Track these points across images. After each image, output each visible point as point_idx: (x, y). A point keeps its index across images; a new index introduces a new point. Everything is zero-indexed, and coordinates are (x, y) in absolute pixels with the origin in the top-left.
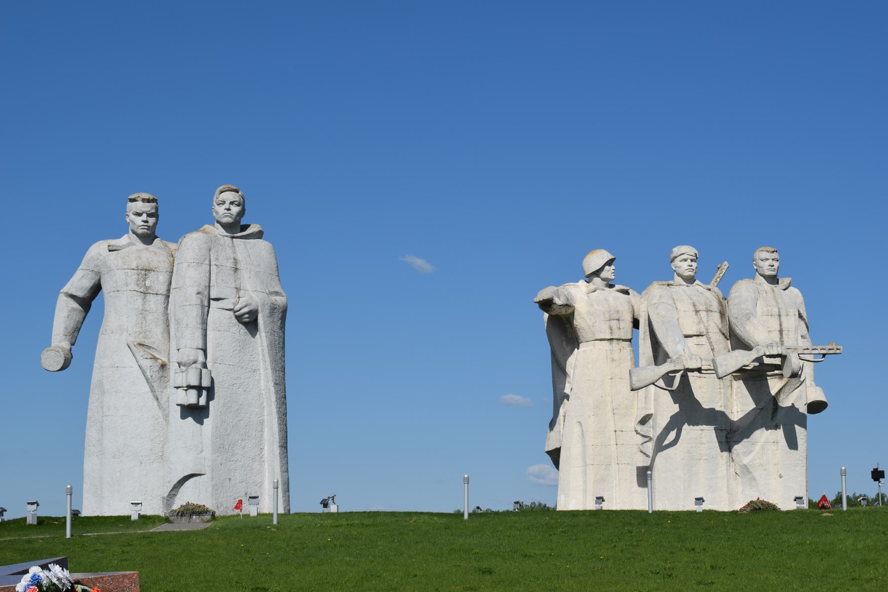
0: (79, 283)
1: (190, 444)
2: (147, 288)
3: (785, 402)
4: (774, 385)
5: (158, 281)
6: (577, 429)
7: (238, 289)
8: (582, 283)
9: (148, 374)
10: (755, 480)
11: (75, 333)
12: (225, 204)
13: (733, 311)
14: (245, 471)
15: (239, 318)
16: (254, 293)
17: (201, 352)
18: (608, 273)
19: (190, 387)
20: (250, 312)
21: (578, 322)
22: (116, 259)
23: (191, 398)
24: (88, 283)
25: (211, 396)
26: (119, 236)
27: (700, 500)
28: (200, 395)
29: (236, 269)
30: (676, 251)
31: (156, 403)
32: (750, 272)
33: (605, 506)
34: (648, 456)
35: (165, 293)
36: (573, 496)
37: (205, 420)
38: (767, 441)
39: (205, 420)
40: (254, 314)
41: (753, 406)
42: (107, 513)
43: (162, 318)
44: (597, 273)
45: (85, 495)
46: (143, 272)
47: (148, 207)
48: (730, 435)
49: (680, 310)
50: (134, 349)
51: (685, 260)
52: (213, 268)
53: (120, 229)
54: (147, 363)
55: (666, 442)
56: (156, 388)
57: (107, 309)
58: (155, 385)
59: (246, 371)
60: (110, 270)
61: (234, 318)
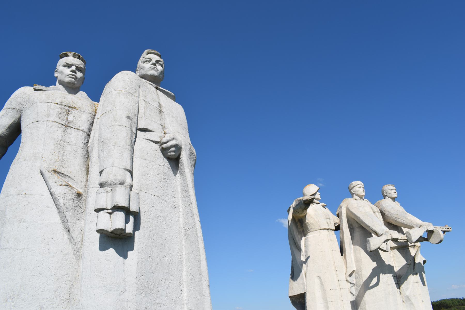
2: (69, 122)
6: (317, 281)
7: (163, 127)
9: (61, 202)
10: (412, 304)
15: (164, 151)
17: (129, 174)
19: (117, 208)
20: (176, 146)
23: (118, 221)
25: (137, 227)
28: (127, 221)
29: (161, 111)
30: (354, 183)
31: (66, 236)
34: (353, 295)
35: (86, 130)
37: (129, 253)
39: (129, 253)
41: (406, 263)
43: (81, 153)
46: (67, 108)
48: (399, 280)
50: (47, 175)
51: (360, 187)
52: (142, 103)
53: (49, 80)
54: (59, 191)
55: (371, 285)
56: (69, 218)
58: (68, 214)
61: (159, 151)
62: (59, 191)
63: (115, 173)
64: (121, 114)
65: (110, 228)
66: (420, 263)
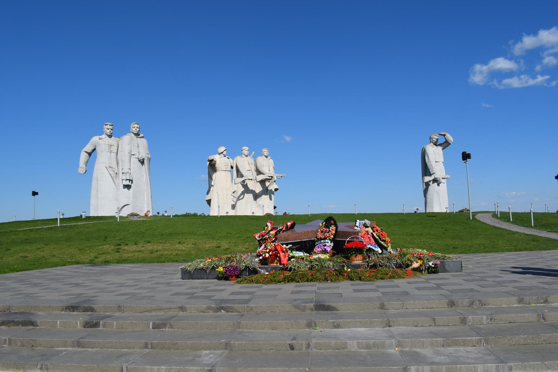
0: (89, 148)
1: (126, 196)
3: (269, 189)
4: (267, 184)
5: (114, 149)
8: (217, 155)
11: (87, 163)
12: (135, 127)
13: (258, 165)
14: (141, 203)
15: (139, 161)
16: (144, 153)
18: (225, 153)
21: (217, 165)
22: (101, 142)
23: (128, 183)
24: (92, 148)
25: (132, 183)
26: (101, 135)
27: (227, 213)
30: (244, 148)
32: (262, 155)
33: (254, 215)
36: (214, 212)
38: (265, 198)
40: (143, 159)
42: (100, 215)
43: (115, 159)
44: (222, 153)
45: (91, 210)
47: (111, 127)
48: (256, 196)
49: (245, 164)
57: (98, 156)
59: (141, 175)
60: (100, 145)
62: (112, 173)
63: (125, 170)
64: (127, 152)
65: (125, 184)
66: (271, 190)
